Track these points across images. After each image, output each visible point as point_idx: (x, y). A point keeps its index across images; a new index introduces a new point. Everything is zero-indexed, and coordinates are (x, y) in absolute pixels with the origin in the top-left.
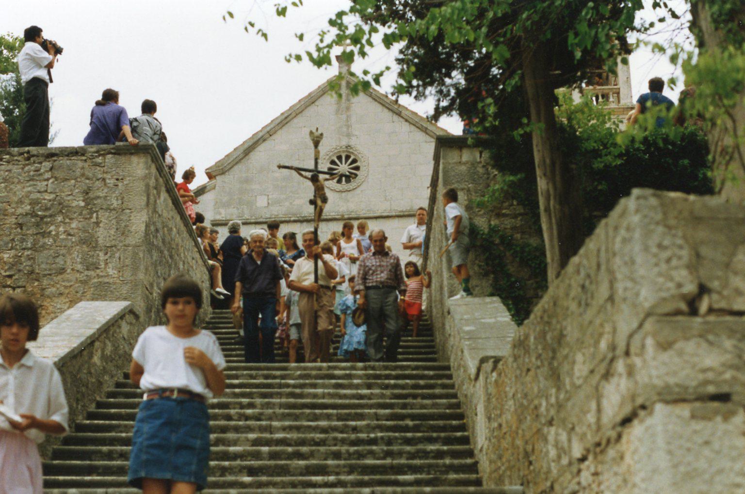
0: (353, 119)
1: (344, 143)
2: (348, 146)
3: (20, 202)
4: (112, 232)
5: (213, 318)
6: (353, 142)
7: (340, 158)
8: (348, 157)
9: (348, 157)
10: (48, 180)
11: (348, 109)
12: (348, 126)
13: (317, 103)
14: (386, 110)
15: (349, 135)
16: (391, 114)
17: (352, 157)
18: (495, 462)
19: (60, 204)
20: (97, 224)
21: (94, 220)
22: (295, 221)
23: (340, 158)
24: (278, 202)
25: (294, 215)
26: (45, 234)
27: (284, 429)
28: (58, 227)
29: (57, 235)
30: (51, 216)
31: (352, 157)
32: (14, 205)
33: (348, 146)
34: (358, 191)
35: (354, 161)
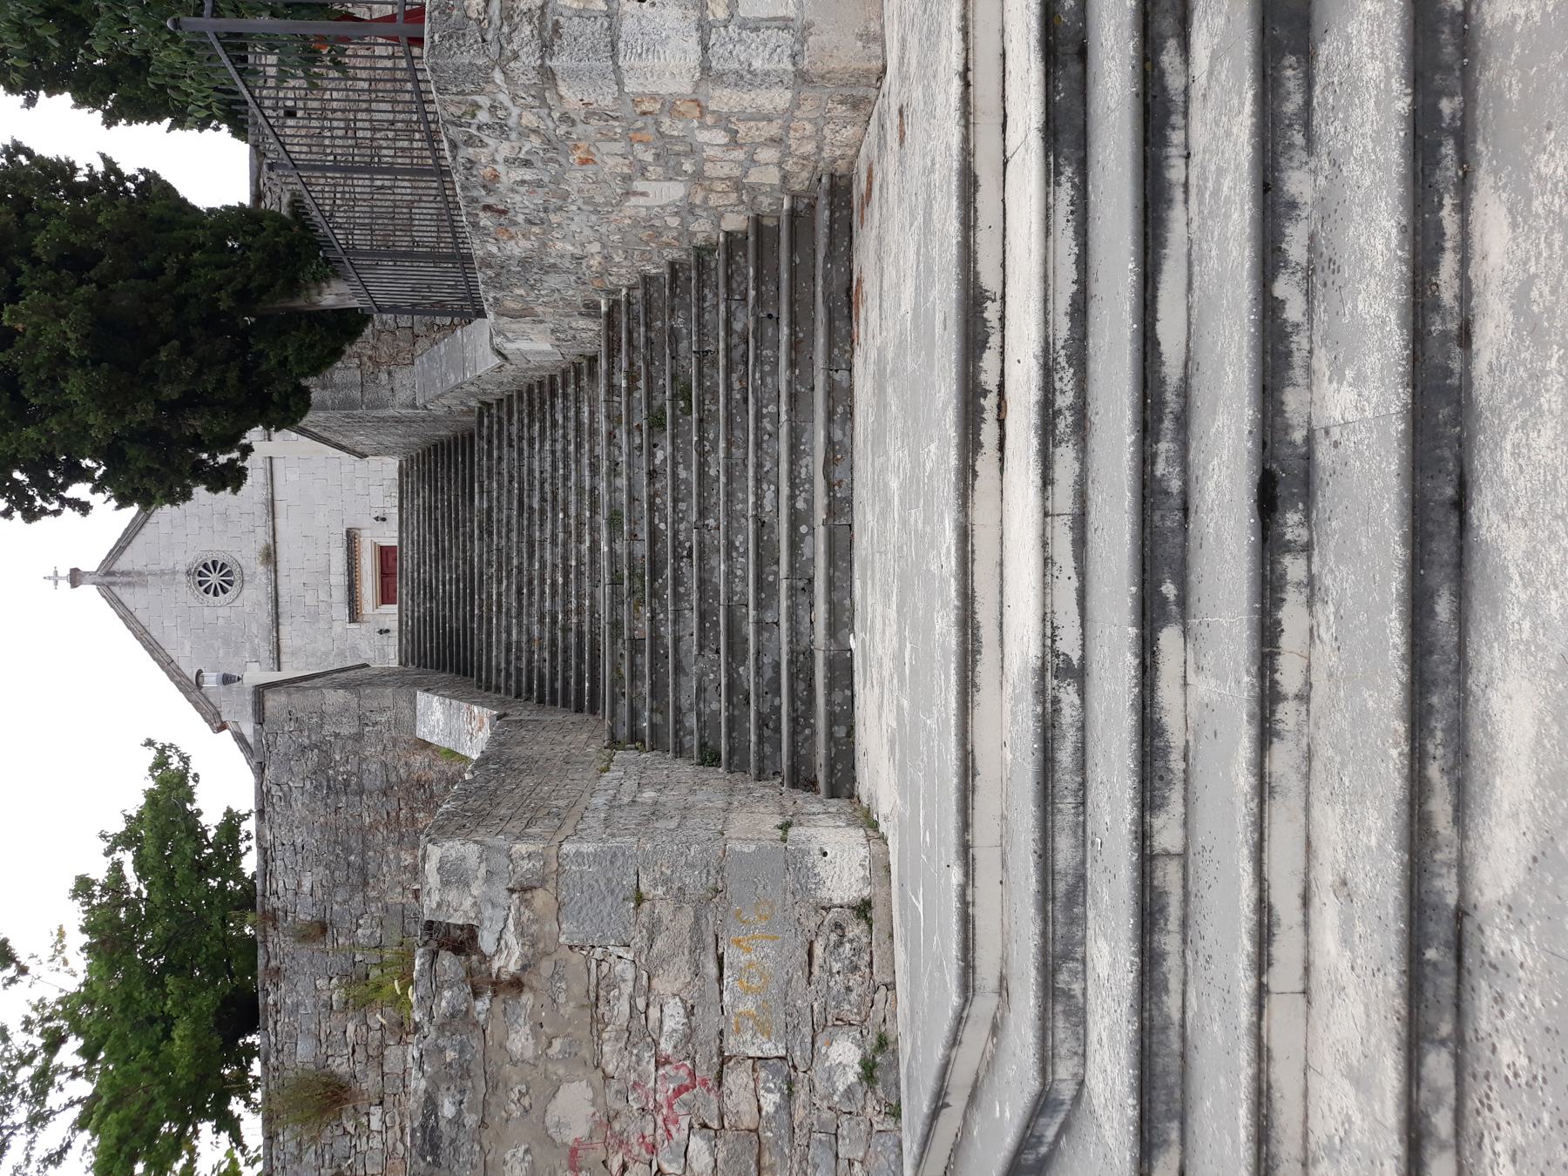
0: (155, 568)
1: (183, 578)
2: (188, 573)
3: (313, 812)
4: (345, 720)
5: (413, 663)
6: (182, 568)
7: (201, 583)
8: (200, 574)
9: (200, 574)
10: (290, 787)
11: (140, 574)
12: (163, 573)
13: (132, 610)
14: (143, 531)
15: (174, 572)
16: (147, 525)
17: (201, 569)
18: (402, 836)
19: (315, 773)
20: (337, 735)
21: (332, 739)
22: (278, 632)
23: (201, 583)
24: (254, 652)
25: (270, 631)
26: (347, 783)
27: (542, 531)
28: (337, 773)
29: (347, 773)
30: (328, 781)
31: (201, 569)
32: (316, 818)
33: (188, 573)
34: (242, 562)
35: (205, 566)
